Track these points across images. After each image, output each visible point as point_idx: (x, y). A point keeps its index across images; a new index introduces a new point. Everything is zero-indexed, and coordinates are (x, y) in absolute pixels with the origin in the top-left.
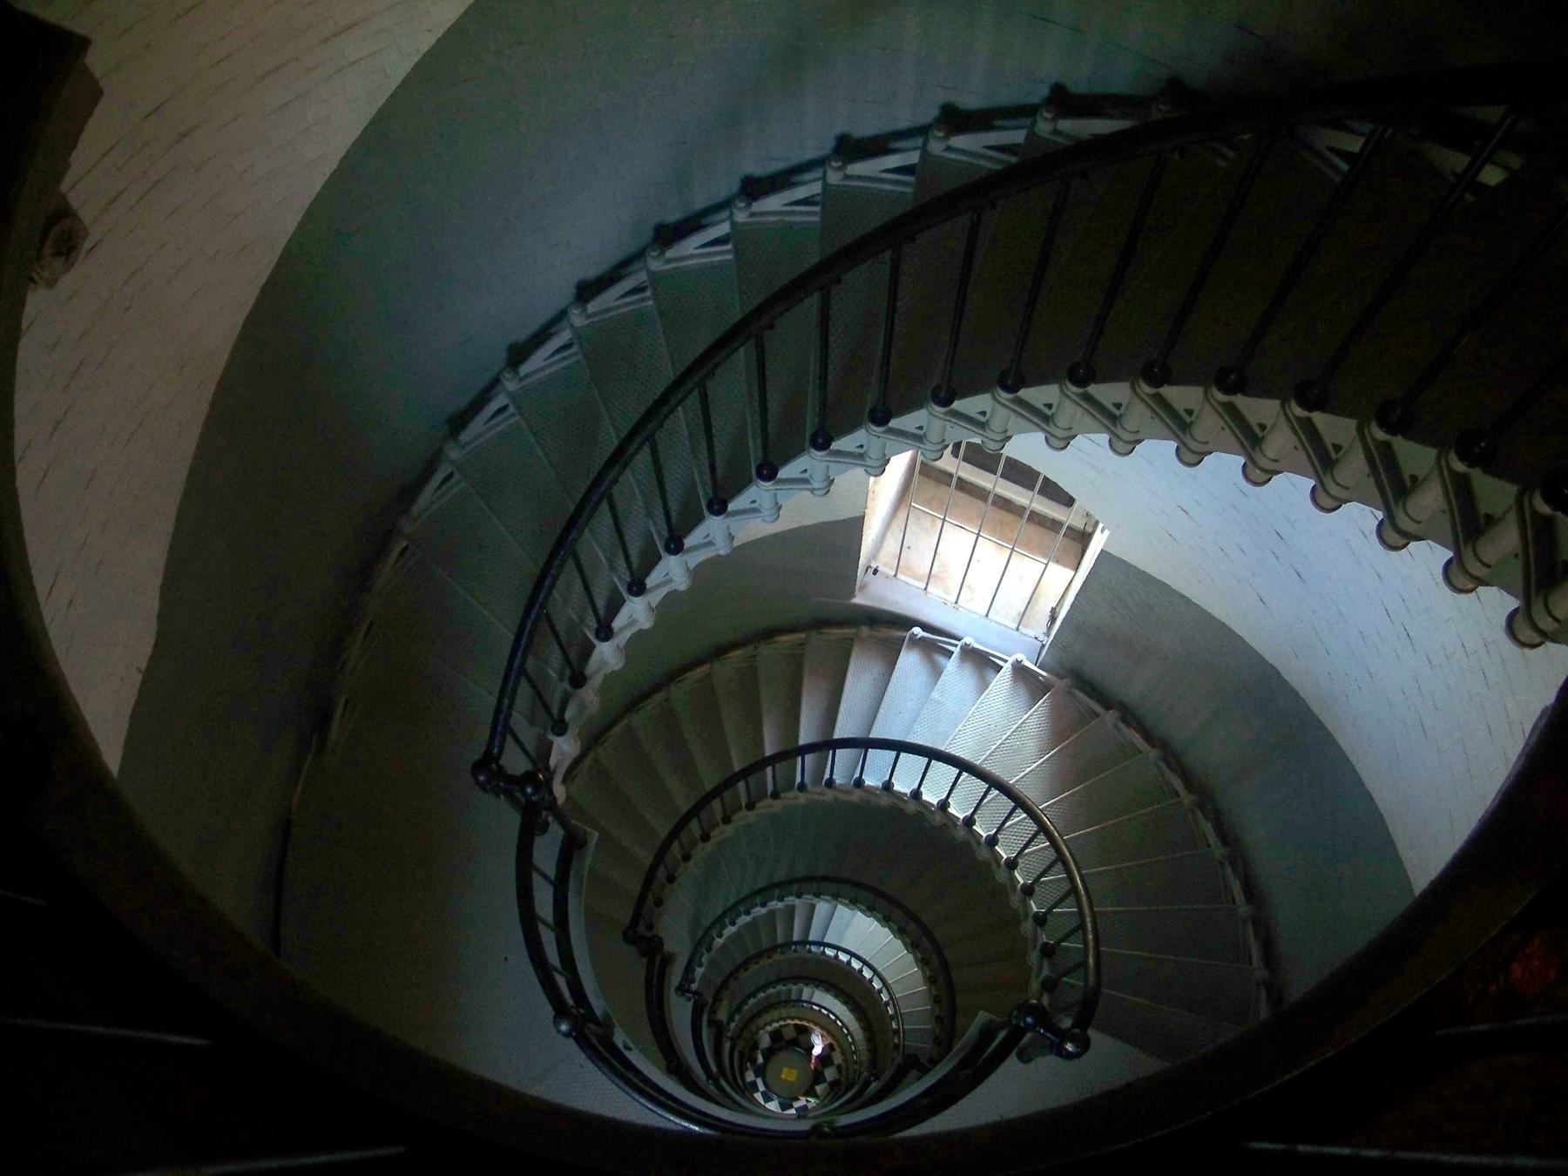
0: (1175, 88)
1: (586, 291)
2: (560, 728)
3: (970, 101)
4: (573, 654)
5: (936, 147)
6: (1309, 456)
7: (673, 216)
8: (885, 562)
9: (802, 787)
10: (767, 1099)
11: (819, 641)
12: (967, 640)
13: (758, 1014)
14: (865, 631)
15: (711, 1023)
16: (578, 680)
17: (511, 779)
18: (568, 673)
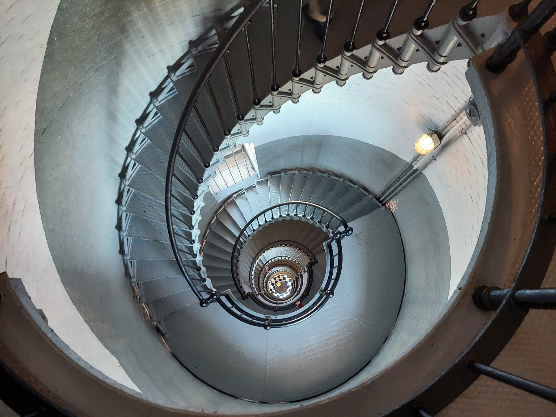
1: (119, 201)
2: (204, 280)
3: (154, 88)
4: (191, 265)
5: (157, 104)
6: (358, 66)
7: (119, 170)
8: (217, 190)
9: (245, 242)
10: (282, 296)
12: (245, 188)
17: (209, 299)
18: (195, 270)
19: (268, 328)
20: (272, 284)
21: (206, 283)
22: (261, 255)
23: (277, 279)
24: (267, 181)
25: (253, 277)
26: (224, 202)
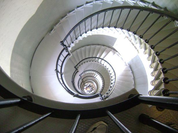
0: (165, 8)
2: (73, 43)
11: (108, 49)
13: (90, 82)
14: (113, 50)
15: (82, 80)
16: (76, 39)
19: (56, 71)
20: (90, 85)
21: (72, 44)
22: (97, 73)
23: (92, 87)
24: (127, 65)
25: (87, 72)
26: (114, 50)
